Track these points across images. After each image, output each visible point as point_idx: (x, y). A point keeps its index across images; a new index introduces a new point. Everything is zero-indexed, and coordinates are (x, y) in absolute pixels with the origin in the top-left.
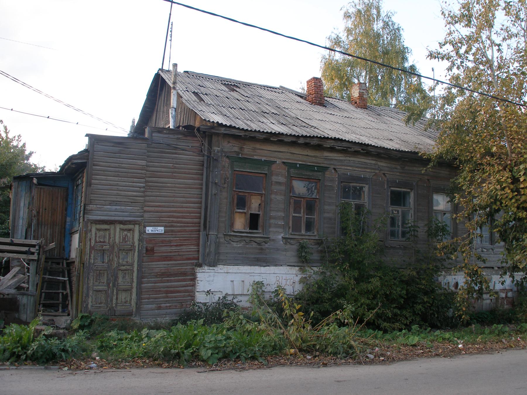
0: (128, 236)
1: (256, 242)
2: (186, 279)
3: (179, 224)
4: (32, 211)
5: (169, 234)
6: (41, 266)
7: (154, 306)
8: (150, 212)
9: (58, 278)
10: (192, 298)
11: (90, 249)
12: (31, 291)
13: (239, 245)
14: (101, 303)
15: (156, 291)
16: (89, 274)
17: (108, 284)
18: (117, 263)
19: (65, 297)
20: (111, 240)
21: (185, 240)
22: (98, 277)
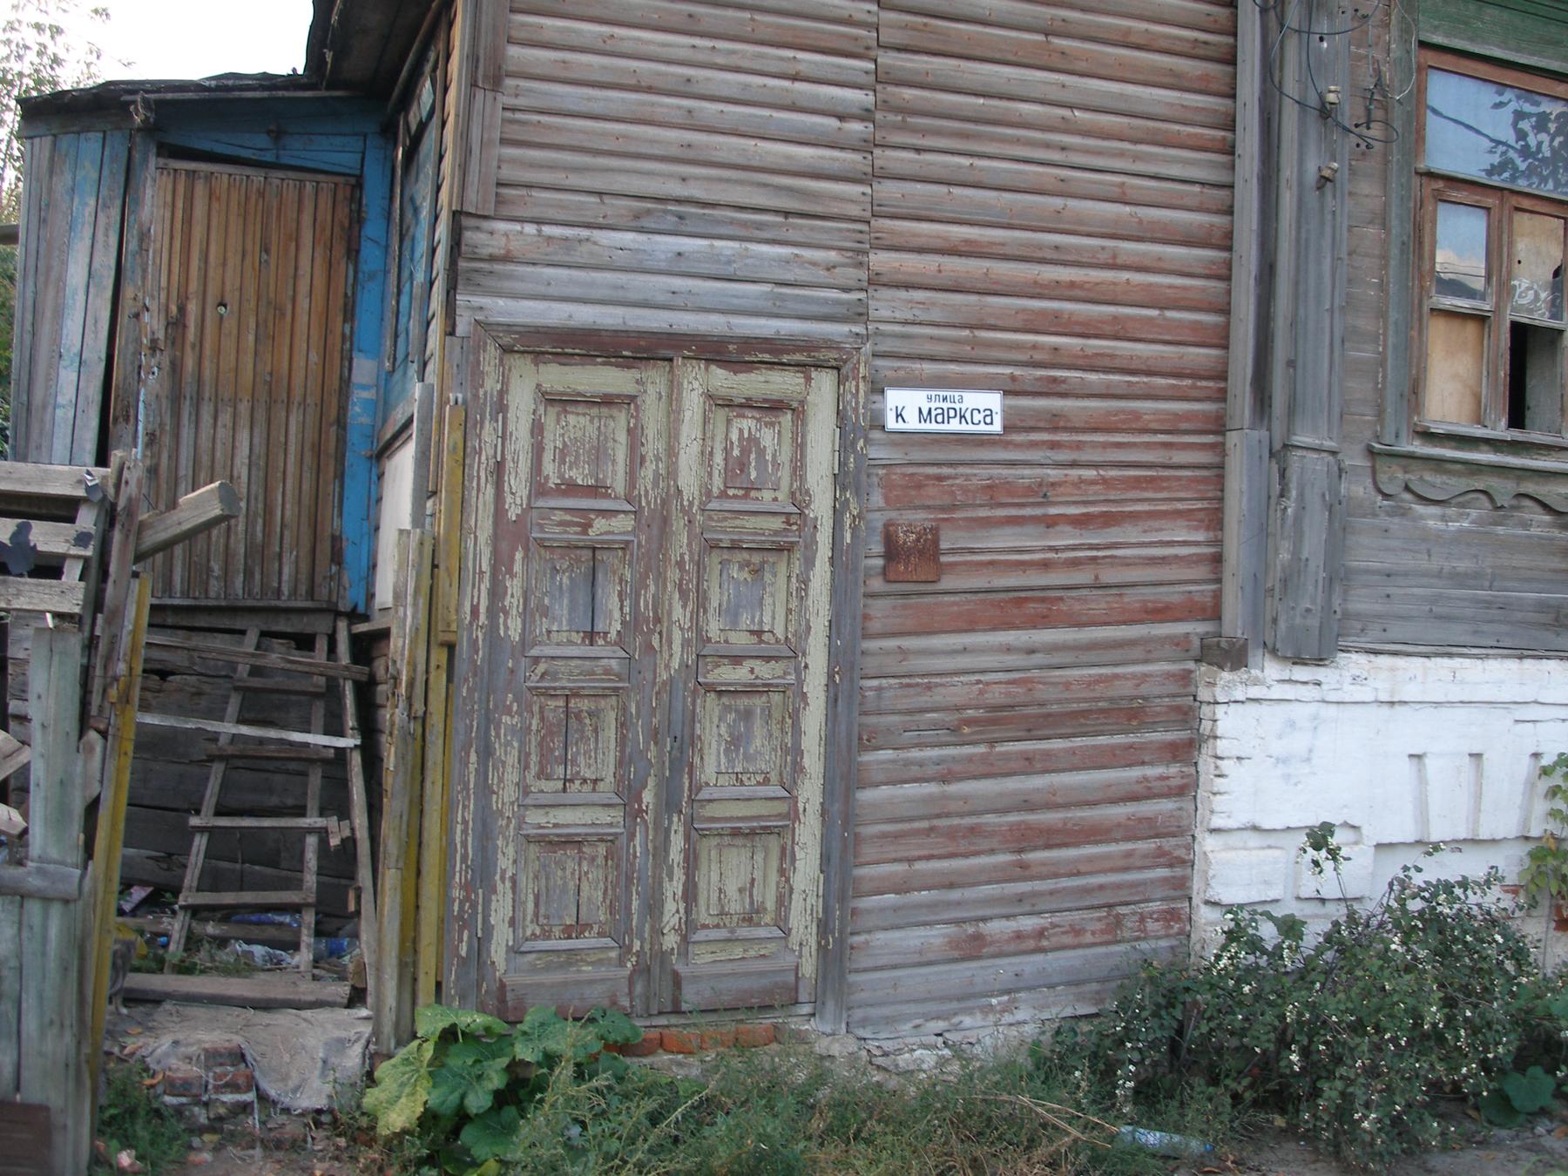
0: (761, 452)
1: (1546, 507)
2: (1142, 747)
3: (1093, 377)
4: (137, 316)
5: (1034, 445)
6: (121, 668)
7: (936, 936)
8: (908, 286)
9: (297, 737)
10: (1178, 871)
11: (496, 538)
12: (41, 859)
13: (1453, 526)
14: (578, 928)
15: (952, 834)
16: (489, 720)
17: (629, 795)
18: (686, 643)
19: (340, 862)
20: (648, 472)
21: (1137, 483)
22: (558, 742)
